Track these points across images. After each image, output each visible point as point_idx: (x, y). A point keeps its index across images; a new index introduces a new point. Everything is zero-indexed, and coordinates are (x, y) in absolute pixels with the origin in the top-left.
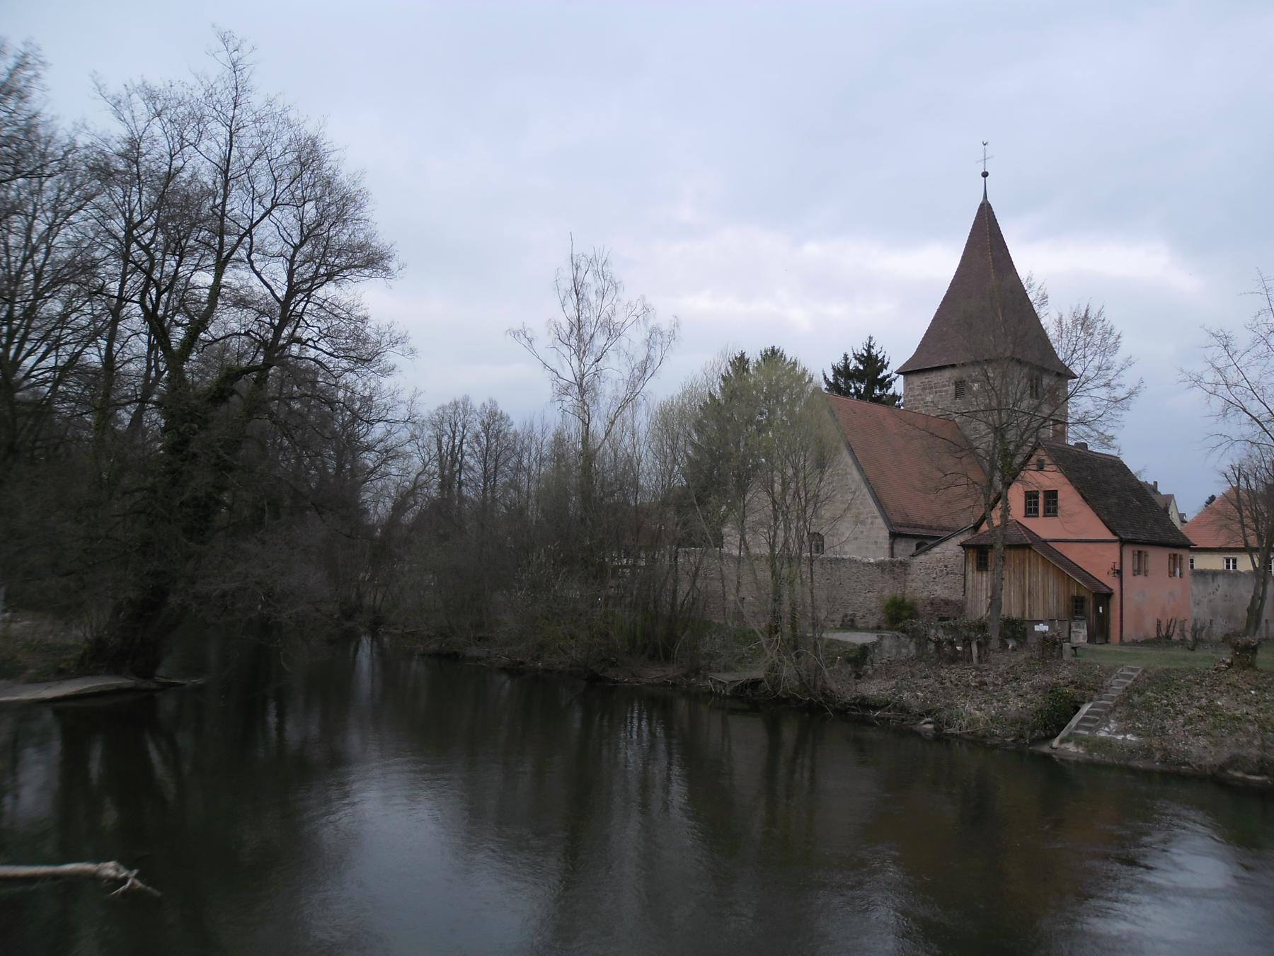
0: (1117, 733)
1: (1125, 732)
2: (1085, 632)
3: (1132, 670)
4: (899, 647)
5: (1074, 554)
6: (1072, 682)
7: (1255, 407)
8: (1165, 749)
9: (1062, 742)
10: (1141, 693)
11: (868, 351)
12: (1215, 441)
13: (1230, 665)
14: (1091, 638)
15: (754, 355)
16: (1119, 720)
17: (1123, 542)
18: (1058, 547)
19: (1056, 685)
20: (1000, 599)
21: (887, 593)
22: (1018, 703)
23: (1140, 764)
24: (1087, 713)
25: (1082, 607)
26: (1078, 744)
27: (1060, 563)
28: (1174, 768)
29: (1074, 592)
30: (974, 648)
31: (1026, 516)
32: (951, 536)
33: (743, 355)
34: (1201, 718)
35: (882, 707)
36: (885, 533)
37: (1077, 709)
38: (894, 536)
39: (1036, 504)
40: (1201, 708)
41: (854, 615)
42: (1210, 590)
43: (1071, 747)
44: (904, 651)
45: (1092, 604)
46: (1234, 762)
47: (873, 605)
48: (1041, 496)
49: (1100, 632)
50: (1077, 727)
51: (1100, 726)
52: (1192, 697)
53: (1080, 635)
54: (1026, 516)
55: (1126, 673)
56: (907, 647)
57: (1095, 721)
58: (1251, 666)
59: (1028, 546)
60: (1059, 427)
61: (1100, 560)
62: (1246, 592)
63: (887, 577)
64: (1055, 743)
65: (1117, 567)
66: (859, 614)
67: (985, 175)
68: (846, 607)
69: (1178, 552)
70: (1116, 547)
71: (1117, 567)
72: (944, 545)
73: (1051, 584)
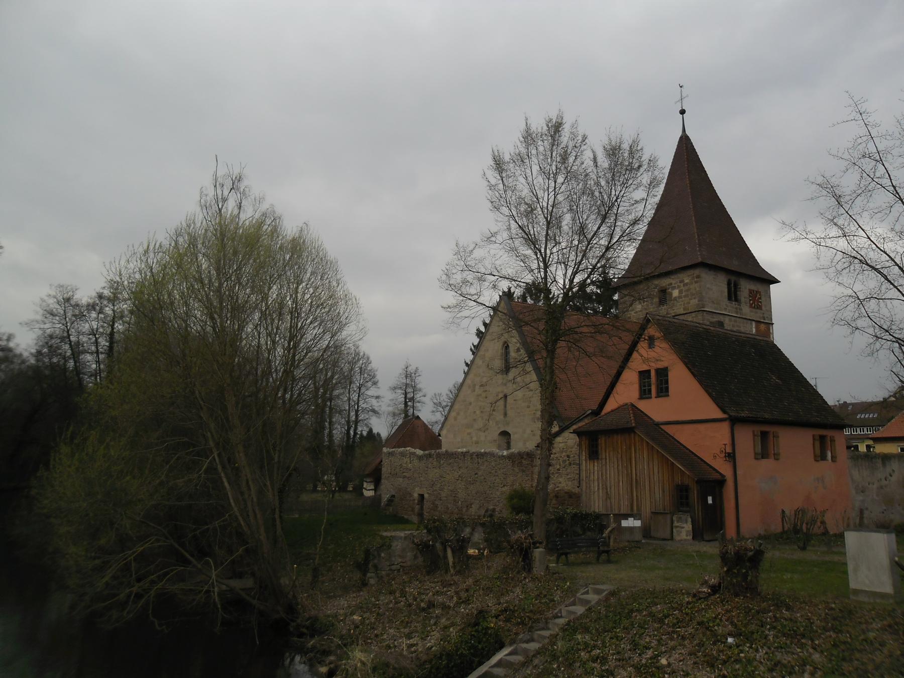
2: (688, 526)
5: (685, 436)
13: (715, 589)
14: (697, 534)
17: (734, 421)
18: (669, 429)
24: (499, 664)
25: (687, 498)
29: (678, 480)
41: (494, 510)
45: (701, 494)
48: (653, 373)
53: (684, 529)
58: (750, 589)
60: (762, 327)
61: (709, 442)
63: (516, 469)
65: (729, 449)
67: (683, 112)
69: (828, 433)
70: (725, 427)
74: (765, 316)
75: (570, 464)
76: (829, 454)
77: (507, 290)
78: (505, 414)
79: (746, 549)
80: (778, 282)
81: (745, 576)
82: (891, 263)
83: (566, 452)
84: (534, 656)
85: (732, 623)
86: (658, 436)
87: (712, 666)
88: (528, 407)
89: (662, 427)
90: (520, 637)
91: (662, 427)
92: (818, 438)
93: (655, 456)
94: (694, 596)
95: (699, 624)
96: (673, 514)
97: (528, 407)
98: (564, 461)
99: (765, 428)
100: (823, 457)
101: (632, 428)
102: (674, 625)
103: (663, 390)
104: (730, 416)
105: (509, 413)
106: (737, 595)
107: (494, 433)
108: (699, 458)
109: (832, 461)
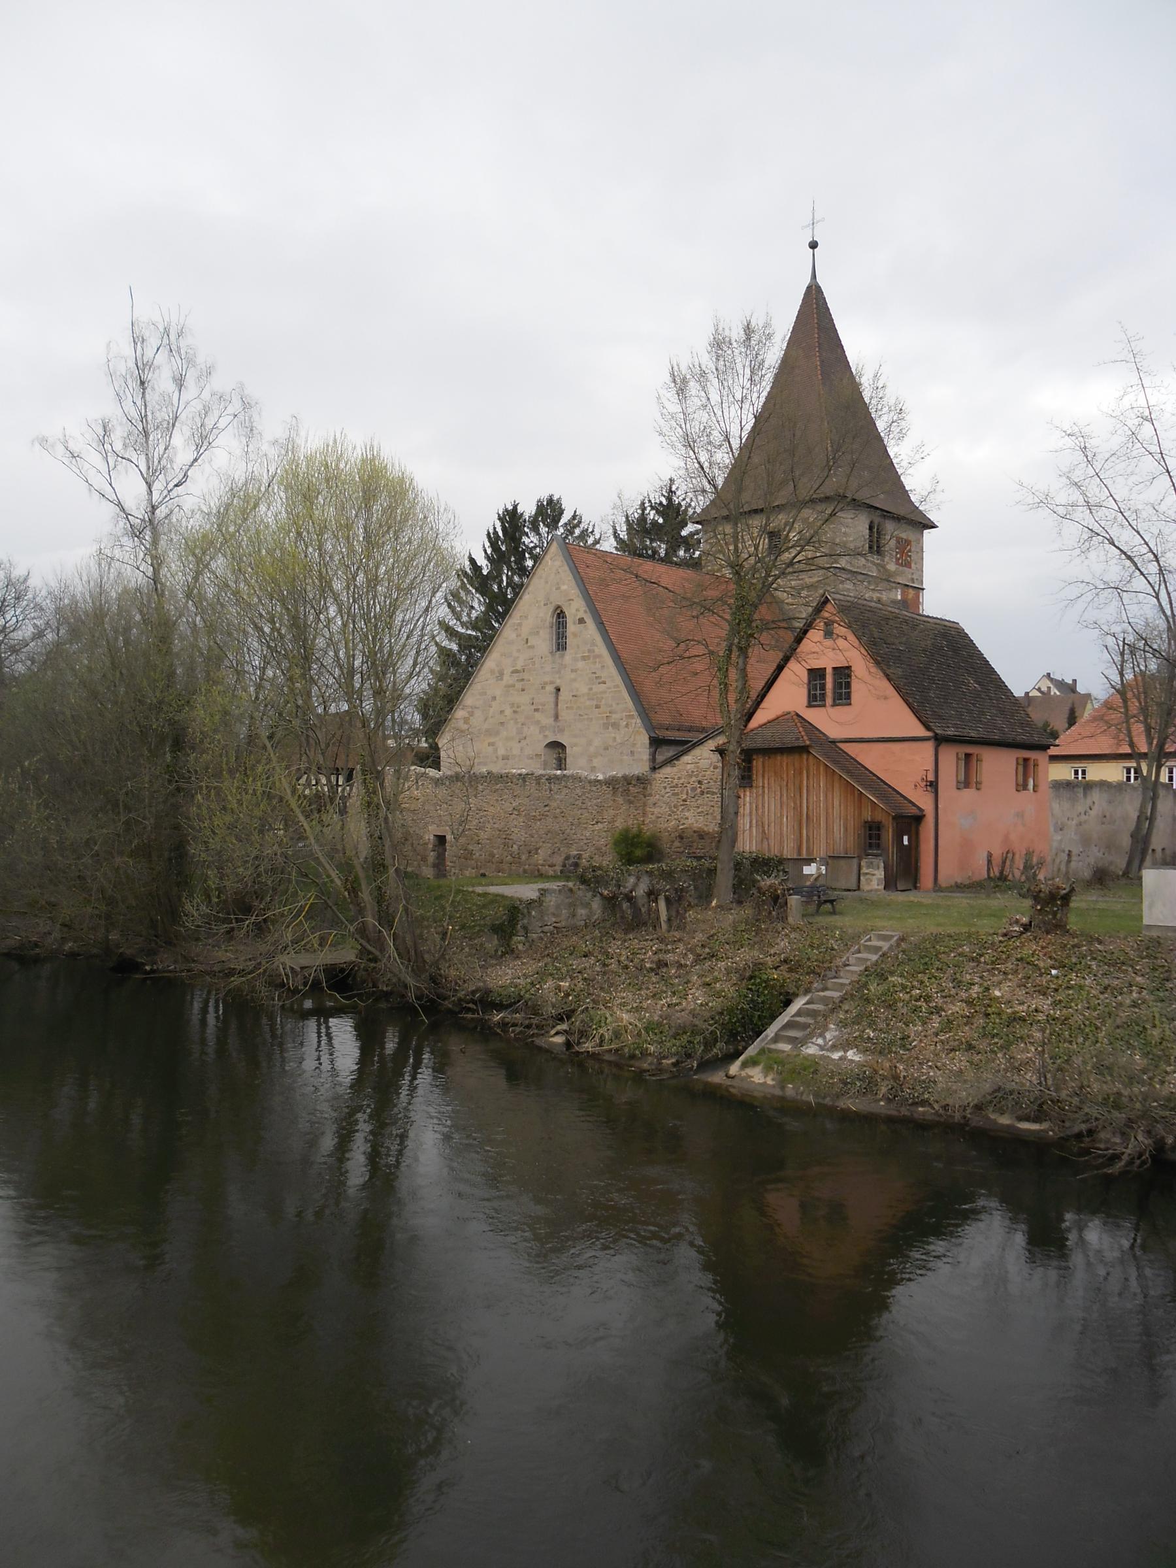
0: (834, 1048)
1: (845, 1046)
2: (880, 874)
3: (885, 938)
4: (572, 905)
5: (871, 758)
6: (785, 961)
7: (1126, 538)
8: (896, 1077)
9: (744, 1065)
10: (882, 977)
11: (669, 499)
12: (1073, 592)
13: (1027, 927)
15: (528, 509)
16: (842, 1024)
18: (848, 748)
19: (759, 966)
20: (734, 828)
21: (620, 824)
22: (698, 1000)
23: (851, 1104)
24: (799, 1013)
25: (879, 837)
26: (768, 1069)
27: (848, 772)
28: (905, 1111)
29: (868, 815)
30: (662, 904)
31: (809, 706)
32: (706, 738)
33: (515, 507)
34: (969, 1020)
35: (507, 1007)
36: (643, 739)
37: (788, 1003)
38: (657, 743)
39: (823, 687)
40: (969, 1002)
41: (579, 857)
42: (1080, 808)
43: (757, 1076)
44: (582, 912)
45: (895, 836)
46: (1000, 1097)
47: (603, 842)
49: (905, 872)
50: (776, 1039)
51: (811, 1036)
52: (958, 984)
53: (874, 877)
54: (809, 706)
55: (875, 943)
56: (587, 905)
57: (805, 1026)
58: (1059, 927)
59: (804, 750)
61: (906, 768)
62: (1130, 807)
63: (620, 800)
64: (734, 1069)
65: (931, 778)
66: (586, 855)
67: (813, 245)
68: (569, 846)
70: (929, 747)
71: (931, 778)
72: (697, 752)
73: (836, 803)
74: (915, 577)
75: (702, 793)
76: (1031, 786)
77: (510, 508)
78: (556, 717)
79: (1058, 888)
80: (934, 526)
81: (1055, 914)
82: (1144, 549)
83: (697, 776)
84: (841, 1002)
85: (1050, 958)
86: (836, 759)
87: (1044, 994)
88: (597, 707)
89: (841, 745)
90: (815, 985)
91: (841, 745)
92: (1021, 762)
93: (837, 785)
94: (1005, 935)
95: (1018, 960)
96: (860, 858)
97: (597, 707)
98: (694, 789)
99: (970, 749)
100: (1025, 787)
101: (797, 747)
102: (993, 963)
103: (843, 695)
104: (936, 734)
105: (564, 714)
106: (1048, 933)
107: (537, 742)
108: (890, 786)
109: (1034, 791)
